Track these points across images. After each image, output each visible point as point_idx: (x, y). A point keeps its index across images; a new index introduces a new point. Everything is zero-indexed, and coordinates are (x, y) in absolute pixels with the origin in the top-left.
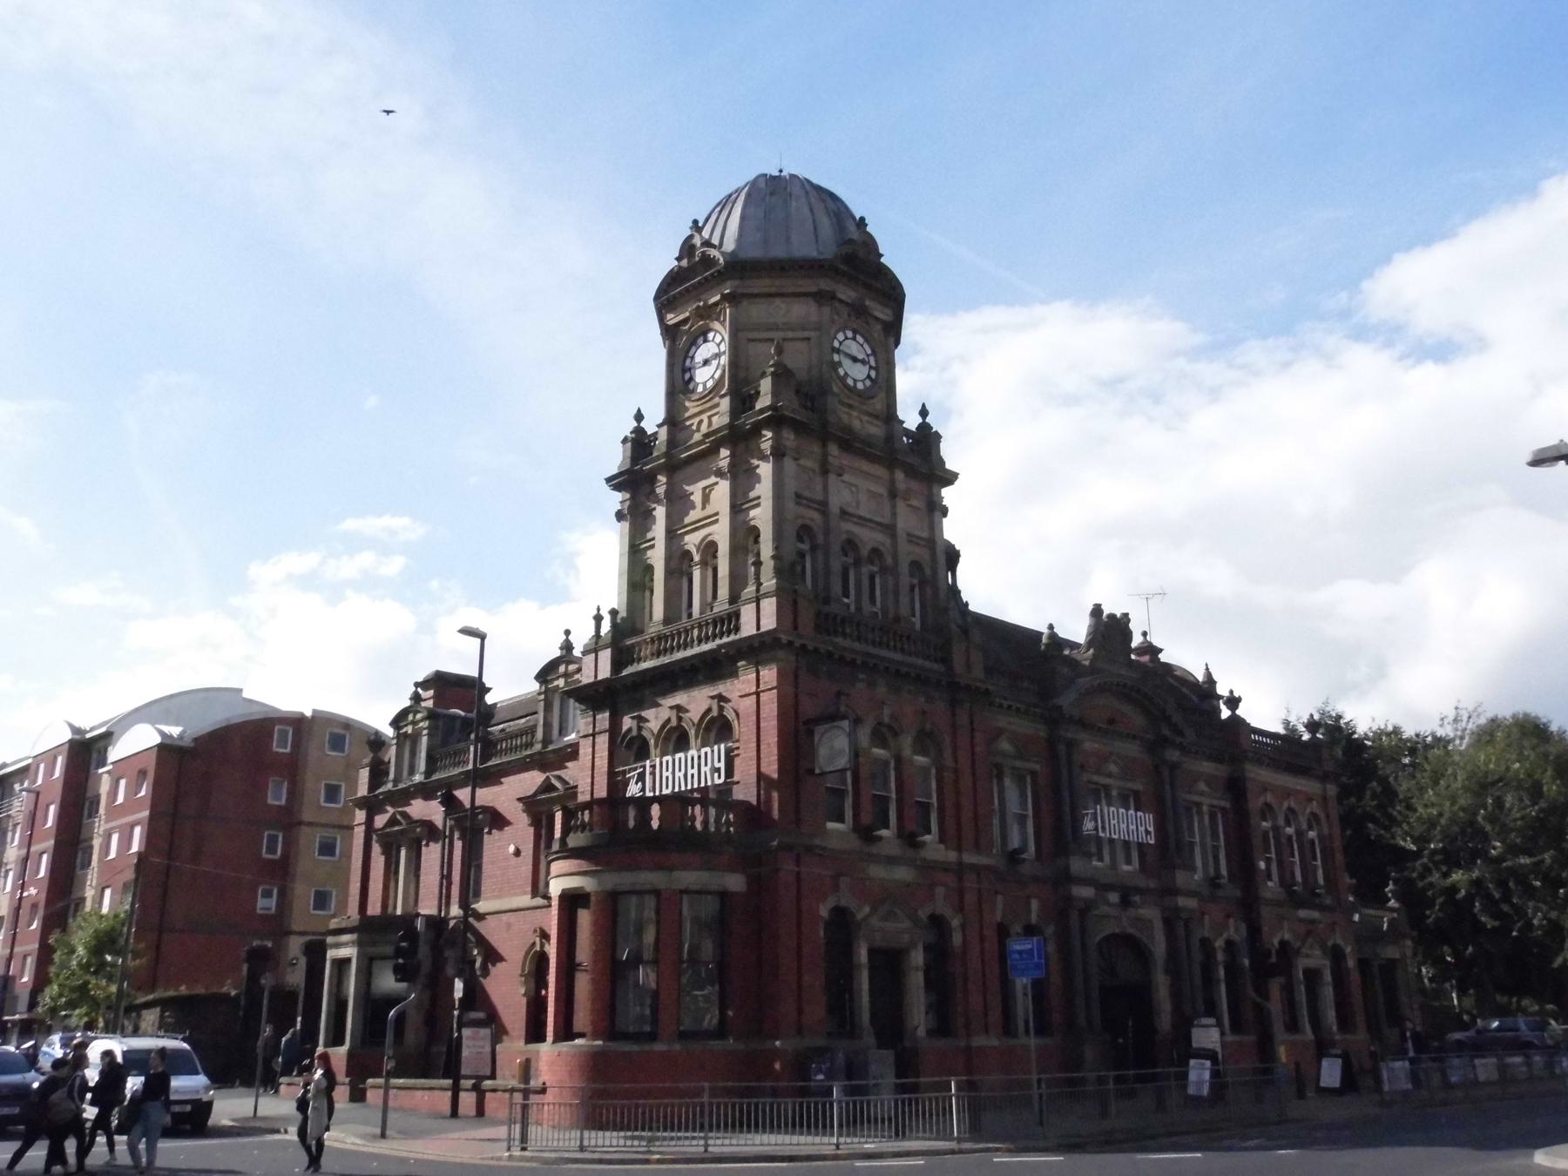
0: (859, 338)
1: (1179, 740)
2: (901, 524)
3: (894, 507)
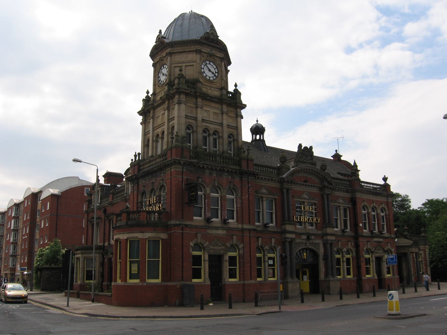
0: (211, 63)
1: (330, 186)
2: (225, 122)
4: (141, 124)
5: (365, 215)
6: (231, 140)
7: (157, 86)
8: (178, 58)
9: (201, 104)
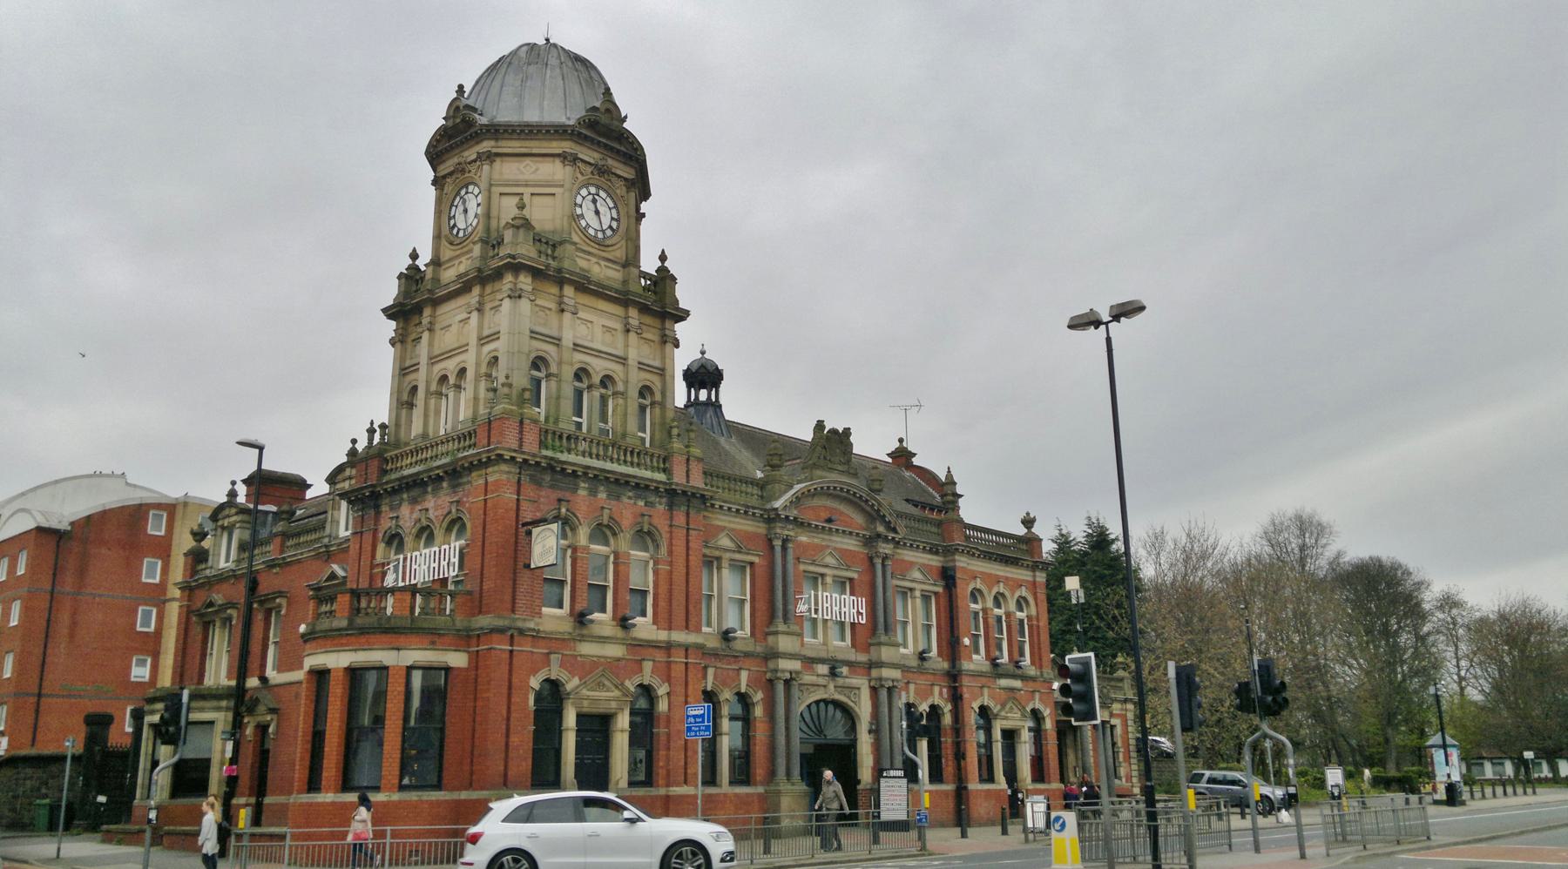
1: (891, 535)
2: (633, 355)
3: (626, 340)
4: (393, 342)
5: (976, 614)
6: (647, 402)
7: (444, 242)
8: (508, 170)
9: (572, 302)
